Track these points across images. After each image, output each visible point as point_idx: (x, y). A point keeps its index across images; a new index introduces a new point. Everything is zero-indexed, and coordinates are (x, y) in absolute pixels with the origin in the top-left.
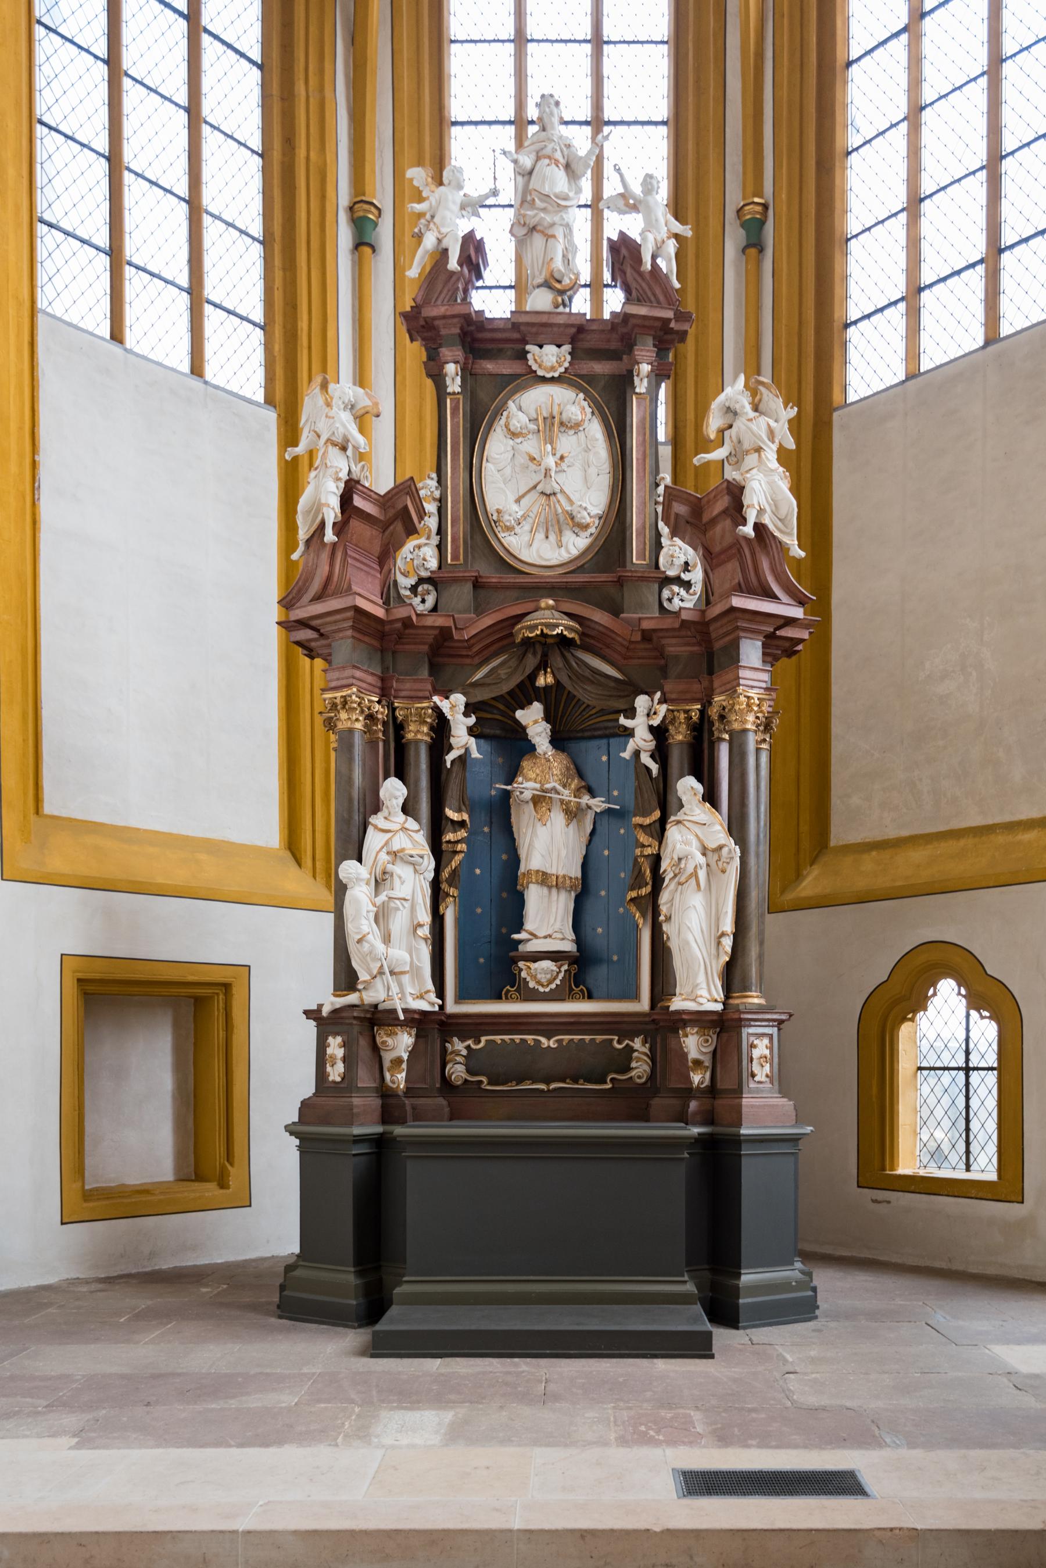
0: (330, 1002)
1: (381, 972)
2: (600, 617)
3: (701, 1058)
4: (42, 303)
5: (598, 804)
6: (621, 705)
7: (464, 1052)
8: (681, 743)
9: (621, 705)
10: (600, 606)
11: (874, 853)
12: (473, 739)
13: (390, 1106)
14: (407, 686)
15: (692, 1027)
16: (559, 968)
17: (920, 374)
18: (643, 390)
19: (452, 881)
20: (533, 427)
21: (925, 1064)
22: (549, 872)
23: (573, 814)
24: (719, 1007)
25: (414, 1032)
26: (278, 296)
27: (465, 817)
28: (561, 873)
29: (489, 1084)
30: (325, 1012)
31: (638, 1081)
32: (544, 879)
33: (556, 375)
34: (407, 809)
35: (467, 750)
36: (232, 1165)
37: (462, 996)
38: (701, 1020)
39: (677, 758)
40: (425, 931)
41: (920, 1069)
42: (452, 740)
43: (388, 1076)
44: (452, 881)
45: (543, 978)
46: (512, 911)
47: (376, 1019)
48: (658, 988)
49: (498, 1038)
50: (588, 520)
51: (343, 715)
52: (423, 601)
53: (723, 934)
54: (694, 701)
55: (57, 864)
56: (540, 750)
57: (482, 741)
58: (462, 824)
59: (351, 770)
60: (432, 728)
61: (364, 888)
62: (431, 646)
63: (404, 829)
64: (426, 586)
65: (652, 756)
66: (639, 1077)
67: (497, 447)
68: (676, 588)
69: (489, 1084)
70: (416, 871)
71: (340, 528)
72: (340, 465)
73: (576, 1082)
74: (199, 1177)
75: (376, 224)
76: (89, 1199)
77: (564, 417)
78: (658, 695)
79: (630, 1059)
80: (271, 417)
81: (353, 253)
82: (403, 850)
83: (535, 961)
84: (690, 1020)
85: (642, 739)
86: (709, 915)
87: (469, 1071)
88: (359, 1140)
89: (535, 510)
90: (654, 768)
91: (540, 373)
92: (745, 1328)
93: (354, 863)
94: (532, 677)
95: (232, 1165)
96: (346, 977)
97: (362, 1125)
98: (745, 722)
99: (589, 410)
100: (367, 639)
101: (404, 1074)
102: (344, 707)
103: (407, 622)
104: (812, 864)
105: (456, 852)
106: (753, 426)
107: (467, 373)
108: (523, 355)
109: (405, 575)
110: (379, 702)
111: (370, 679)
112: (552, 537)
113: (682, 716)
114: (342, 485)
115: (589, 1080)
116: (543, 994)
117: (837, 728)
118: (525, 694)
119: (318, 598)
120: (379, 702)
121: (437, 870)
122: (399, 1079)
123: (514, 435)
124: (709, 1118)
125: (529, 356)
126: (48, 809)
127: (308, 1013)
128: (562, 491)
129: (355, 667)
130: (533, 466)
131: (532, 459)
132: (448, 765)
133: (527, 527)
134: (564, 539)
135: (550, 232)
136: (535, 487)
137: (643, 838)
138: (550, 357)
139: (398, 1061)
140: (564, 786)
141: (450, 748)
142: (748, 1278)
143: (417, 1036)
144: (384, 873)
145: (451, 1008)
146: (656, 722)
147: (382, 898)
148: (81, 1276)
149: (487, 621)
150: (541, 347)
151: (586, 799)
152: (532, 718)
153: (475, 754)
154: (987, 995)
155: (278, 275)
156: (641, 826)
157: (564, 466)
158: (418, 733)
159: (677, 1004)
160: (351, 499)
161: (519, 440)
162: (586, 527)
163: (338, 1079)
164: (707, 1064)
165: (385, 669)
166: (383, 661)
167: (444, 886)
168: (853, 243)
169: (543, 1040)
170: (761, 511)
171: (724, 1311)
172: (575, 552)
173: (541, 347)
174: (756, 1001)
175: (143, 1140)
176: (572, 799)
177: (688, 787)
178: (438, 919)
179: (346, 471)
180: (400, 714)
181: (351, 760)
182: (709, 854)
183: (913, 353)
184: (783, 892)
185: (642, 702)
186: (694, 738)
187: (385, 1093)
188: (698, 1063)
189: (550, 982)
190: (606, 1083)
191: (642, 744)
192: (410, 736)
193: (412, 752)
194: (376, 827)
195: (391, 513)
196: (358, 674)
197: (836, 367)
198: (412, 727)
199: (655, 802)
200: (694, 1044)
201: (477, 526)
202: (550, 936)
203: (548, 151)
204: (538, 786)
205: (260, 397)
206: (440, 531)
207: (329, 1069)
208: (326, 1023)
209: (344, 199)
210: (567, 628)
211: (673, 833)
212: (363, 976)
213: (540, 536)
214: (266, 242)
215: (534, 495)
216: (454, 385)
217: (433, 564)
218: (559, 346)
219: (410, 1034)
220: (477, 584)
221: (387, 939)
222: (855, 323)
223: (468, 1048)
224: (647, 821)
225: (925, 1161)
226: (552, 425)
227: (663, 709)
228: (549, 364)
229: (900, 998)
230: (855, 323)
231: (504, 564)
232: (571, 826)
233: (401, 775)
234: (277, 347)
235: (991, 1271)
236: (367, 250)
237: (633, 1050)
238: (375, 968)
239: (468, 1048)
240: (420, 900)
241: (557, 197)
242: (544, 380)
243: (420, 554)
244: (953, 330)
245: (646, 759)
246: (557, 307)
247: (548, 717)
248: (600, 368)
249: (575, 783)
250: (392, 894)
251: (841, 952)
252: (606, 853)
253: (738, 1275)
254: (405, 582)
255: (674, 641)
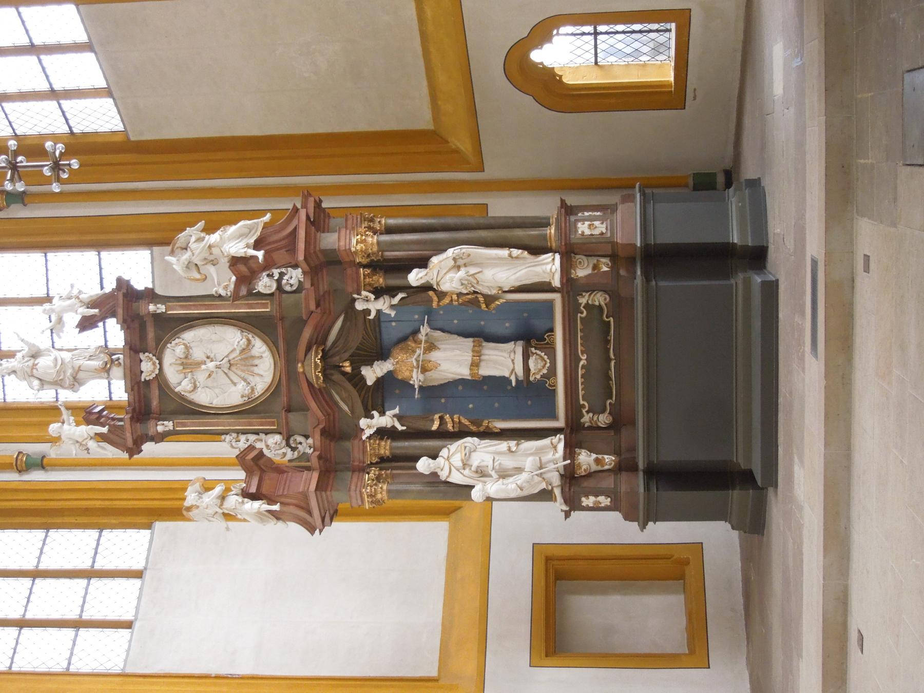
0: (559, 505)
1: (540, 475)
2: (307, 333)
3: (591, 266)
4: (117, 670)
5: (425, 330)
6: (361, 319)
7: (591, 415)
8: (385, 279)
9: (361, 319)
10: (300, 333)
11: (439, 103)
12: (388, 413)
13: (625, 466)
14: (357, 454)
15: (571, 273)
16: (533, 354)
17: (109, 87)
18: (164, 307)
19: (477, 423)
20: (189, 375)
21: (593, 60)
22: (470, 362)
23: (431, 347)
24: (557, 256)
25: (577, 450)
26: (80, 520)
27: (437, 416)
28: (471, 354)
29: (611, 398)
30: (566, 508)
31: (608, 299)
32: (475, 365)
33: (157, 362)
34: (434, 457)
35: (394, 416)
36: (672, 556)
37: (554, 417)
38: (566, 268)
39: (394, 282)
40: (513, 444)
41: (596, 63)
42: (389, 426)
43: (606, 467)
44: (477, 423)
45: (540, 364)
46: (498, 383)
47: (571, 478)
48: (546, 288)
49: (581, 393)
50: (244, 340)
51: (379, 496)
52: (301, 443)
53: (510, 255)
54: (358, 273)
55: (470, 668)
56: (391, 368)
57: (386, 405)
58: (441, 418)
59: (413, 491)
60: (382, 439)
61: (488, 486)
62: (331, 441)
63: (448, 459)
64: (291, 442)
65: (394, 296)
66: (605, 299)
67: (203, 398)
68: (284, 282)
69: (611, 398)
70: (475, 451)
71: (271, 501)
72: (233, 500)
73: (608, 342)
74: (682, 577)
75: (28, 455)
76: (695, 651)
77: (182, 356)
78: (355, 296)
79: (593, 306)
80: (158, 525)
81: (47, 471)
82: (462, 461)
83: (530, 370)
84: (567, 275)
85: (383, 305)
86: (496, 265)
87: (603, 411)
88: (647, 488)
89: (240, 373)
90: (400, 296)
91: (157, 372)
92: (767, 242)
93: (473, 491)
94: (344, 374)
95: (672, 556)
96: (545, 495)
97: (638, 485)
98: (372, 244)
99: (177, 340)
100: (331, 482)
101: (606, 457)
102: (374, 496)
103: (320, 457)
104: (447, 142)
105: (460, 422)
106: (197, 252)
107: (162, 416)
108: (147, 383)
109: (285, 454)
110: (368, 473)
111: (355, 480)
112: (256, 362)
113: (367, 280)
114: (246, 500)
115: (609, 332)
116: (553, 365)
117: (348, 128)
118: (356, 379)
119: (310, 513)
120: (368, 473)
121: (472, 434)
122: (609, 460)
123: (195, 387)
124: (631, 261)
125: (147, 379)
126: (434, 673)
127: (567, 515)
128: (227, 356)
129: (349, 491)
130: (214, 375)
131: (210, 376)
132: (404, 428)
133: (250, 378)
134: (257, 354)
135: (77, 369)
136: (226, 374)
137: (446, 301)
138: (148, 368)
139: (597, 461)
140: (414, 352)
141: (393, 427)
142: (735, 239)
143: (581, 447)
144: (477, 472)
145: (561, 423)
146: (372, 297)
147: (493, 473)
148: (745, 657)
149: (313, 405)
150: (142, 372)
151: (422, 336)
152: (372, 374)
153: (397, 411)
154: (542, 32)
155: (67, 520)
156: (439, 302)
157: (212, 356)
158: (385, 448)
159: (556, 283)
160: (252, 494)
161: (198, 384)
162: (249, 341)
163: (609, 499)
164: (595, 261)
165: (348, 469)
166: (341, 471)
167: (482, 429)
168: (18, 133)
169: (581, 363)
170: (248, 246)
171: (757, 256)
172: (264, 348)
173: (142, 372)
174: (553, 231)
175: (654, 615)
176: (423, 345)
177: (415, 277)
178: (504, 435)
179: (237, 497)
180: (375, 460)
181: (406, 491)
182: (458, 263)
183: (94, 93)
184: (468, 163)
185: (359, 306)
186: (381, 269)
187: (619, 469)
188: (595, 267)
189: (543, 359)
190: (609, 322)
191: (387, 305)
192: (388, 453)
193: (398, 452)
194: (448, 477)
195: (255, 468)
196: (353, 487)
197: (100, 140)
198: (382, 452)
199: (423, 295)
200: (582, 272)
201: (251, 412)
202: (513, 361)
203: (29, 371)
204: (415, 370)
205: (146, 533)
206: (256, 433)
207: (603, 505)
208: (573, 504)
209: (13, 476)
210: (316, 356)
211: (445, 287)
212: (543, 486)
213: (256, 369)
214: (47, 527)
215: (231, 374)
216: (169, 425)
217: (278, 438)
218: (141, 361)
219: (579, 454)
220: (289, 410)
221: (519, 470)
222: (70, 128)
223: (588, 412)
224: (435, 298)
225: (664, 57)
226: (188, 364)
227: (364, 293)
228: (152, 367)
229: (548, 88)
230: (70, 128)
231: (275, 391)
232: (440, 346)
233: (416, 459)
234: (113, 521)
235: (741, 25)
236: (45, 461)
237: (587, 304)
238: (537, 479)
239: (588, 412)
240: (493, 449)
241: (56, 366)
242: (161, 369)
243: (272, 446)
244: (86, 70)
245: (396, 301)
246: (120, 364)
247: (370, 363)
248: (151, 334)
249: (411, 343)
250: (490, 467)
251: (515, 135)
252: (456, 322)
253: (734, 244)
254: (290, 455)
255: (321, 286)
